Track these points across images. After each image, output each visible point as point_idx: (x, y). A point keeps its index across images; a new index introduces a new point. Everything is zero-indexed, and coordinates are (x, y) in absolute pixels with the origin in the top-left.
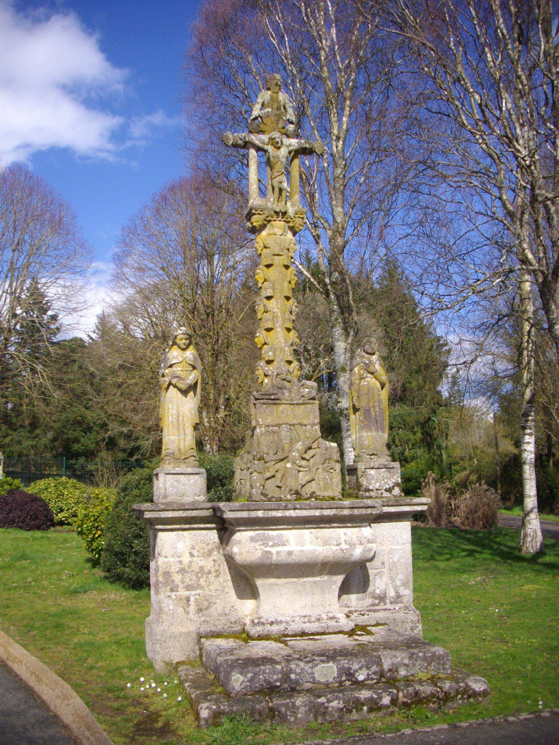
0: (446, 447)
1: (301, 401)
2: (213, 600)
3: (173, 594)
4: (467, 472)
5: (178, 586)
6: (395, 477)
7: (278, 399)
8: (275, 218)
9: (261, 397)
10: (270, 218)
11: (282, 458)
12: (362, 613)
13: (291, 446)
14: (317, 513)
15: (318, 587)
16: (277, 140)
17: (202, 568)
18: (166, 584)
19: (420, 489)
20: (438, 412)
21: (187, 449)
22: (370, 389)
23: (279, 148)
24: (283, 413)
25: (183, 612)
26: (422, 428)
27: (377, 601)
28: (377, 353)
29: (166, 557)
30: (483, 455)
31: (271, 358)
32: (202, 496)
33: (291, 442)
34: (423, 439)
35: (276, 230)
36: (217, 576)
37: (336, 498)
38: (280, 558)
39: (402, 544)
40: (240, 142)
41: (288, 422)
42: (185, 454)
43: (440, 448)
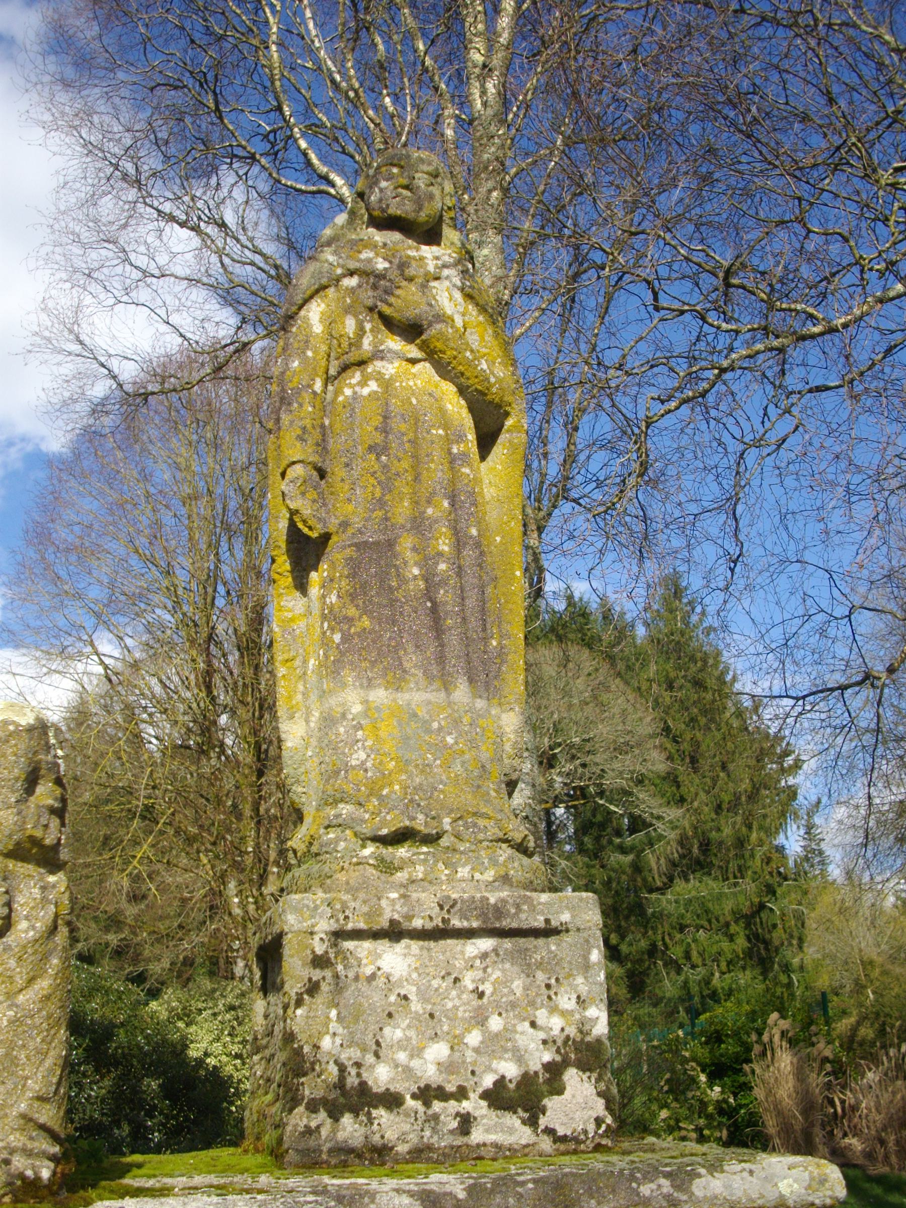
0: (802, 968)
4: (853, 1020)
6: (567, 1002)
19: (748, 1061)
20: (779, 891)
26: (748, 926)
30: (887, 980)
34: (750, 949)
43: (786, 968)
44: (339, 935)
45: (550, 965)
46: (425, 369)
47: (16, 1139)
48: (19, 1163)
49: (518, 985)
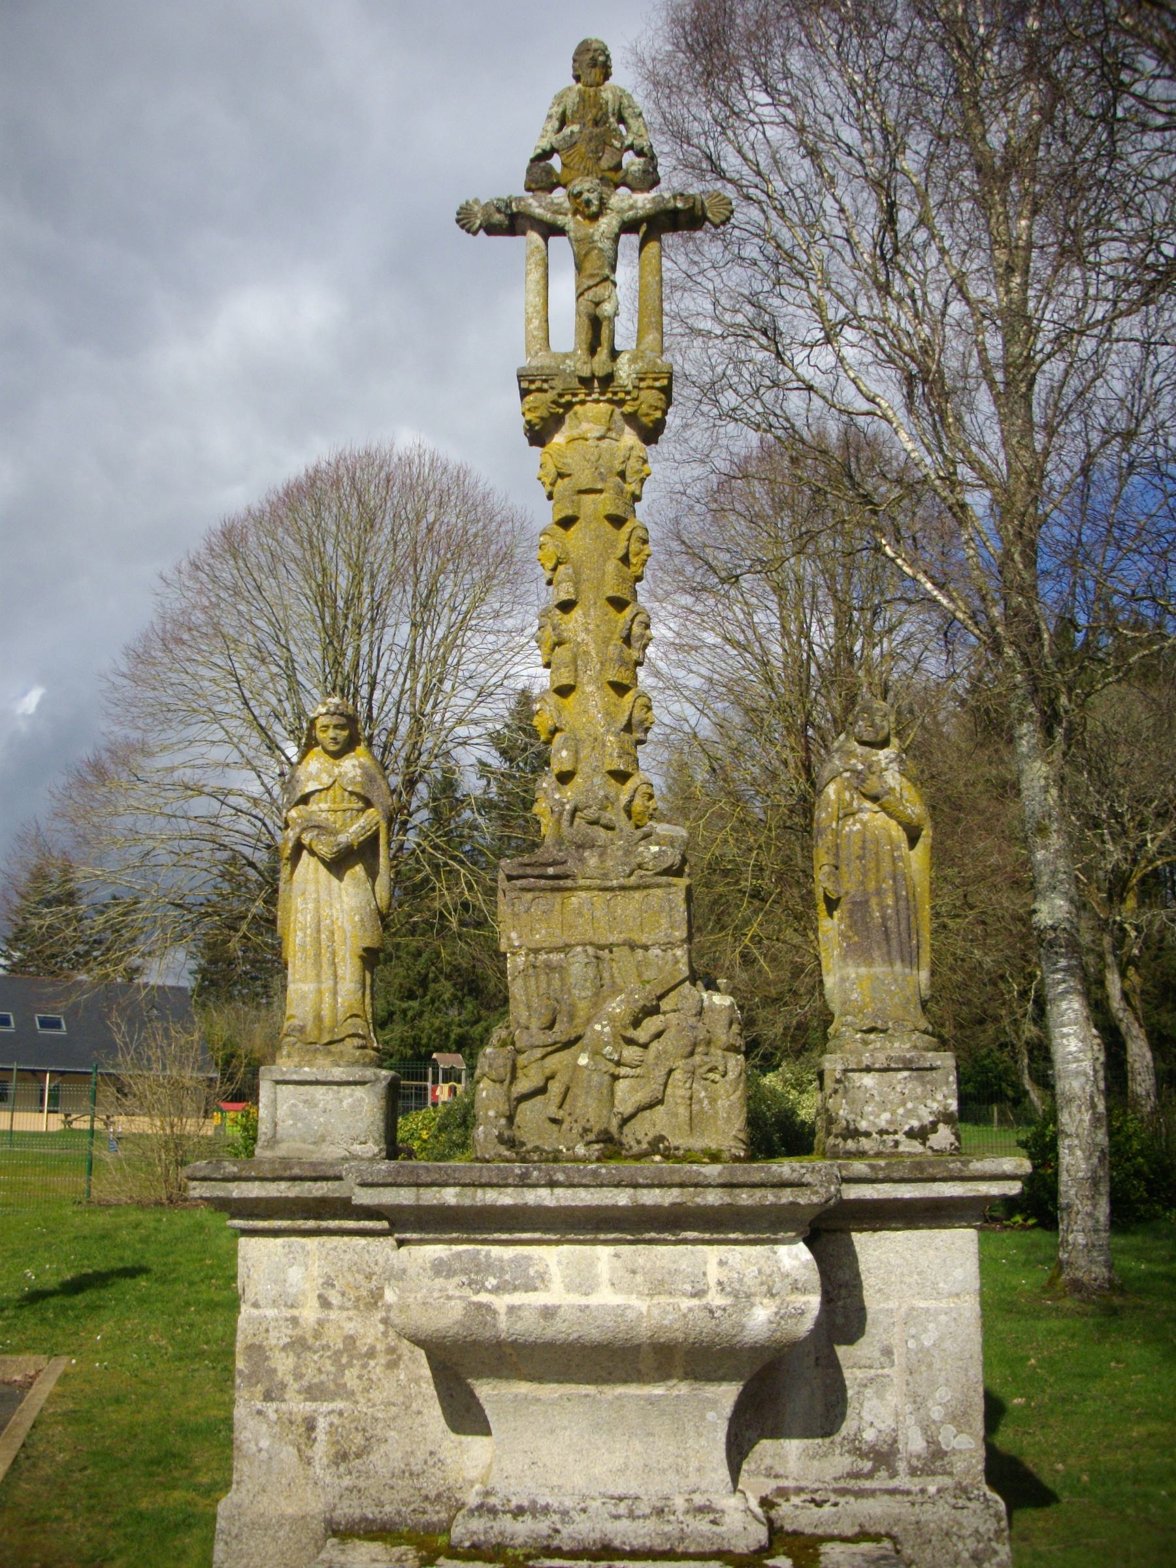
1: (633, 880)
2: (378, 1431)
3: (270, 1408)
5: (284, 1386)
6: (939, 1097)
7: (567, 877)
8: (581, 397)
9: (520, 872)
10: (568, 398)
11: (564, 1038)
12: (817, 1497)
13: (595, 1005)
14: (622, 1198)
15: (663, 1413)
16: (586, 196)
17: (350, 1340)
18: (252, 1378)
21: (341, 1017)
22: (868, 845)
23: (594, 218)
24: (580, 914)
25: (295, 1459)
27: (867, 1465)
28: (895, 741)
29: (256, 1305)
31: (567, 767)
32: (370, 1144)
33: (596, 994)
35: (585, 426)
36: (392, 1365)
37: (726, 1155)
38: (519, 1327)
39: (950, 1295)
40: (498, 218)
41: (595, 940)
42: (332, 1031)
44: (846, 1071)
45: (933, 1082)
46: (882, 815)
47: (732, 1143)
48: (734, 1151)
49: (919, 1090)
